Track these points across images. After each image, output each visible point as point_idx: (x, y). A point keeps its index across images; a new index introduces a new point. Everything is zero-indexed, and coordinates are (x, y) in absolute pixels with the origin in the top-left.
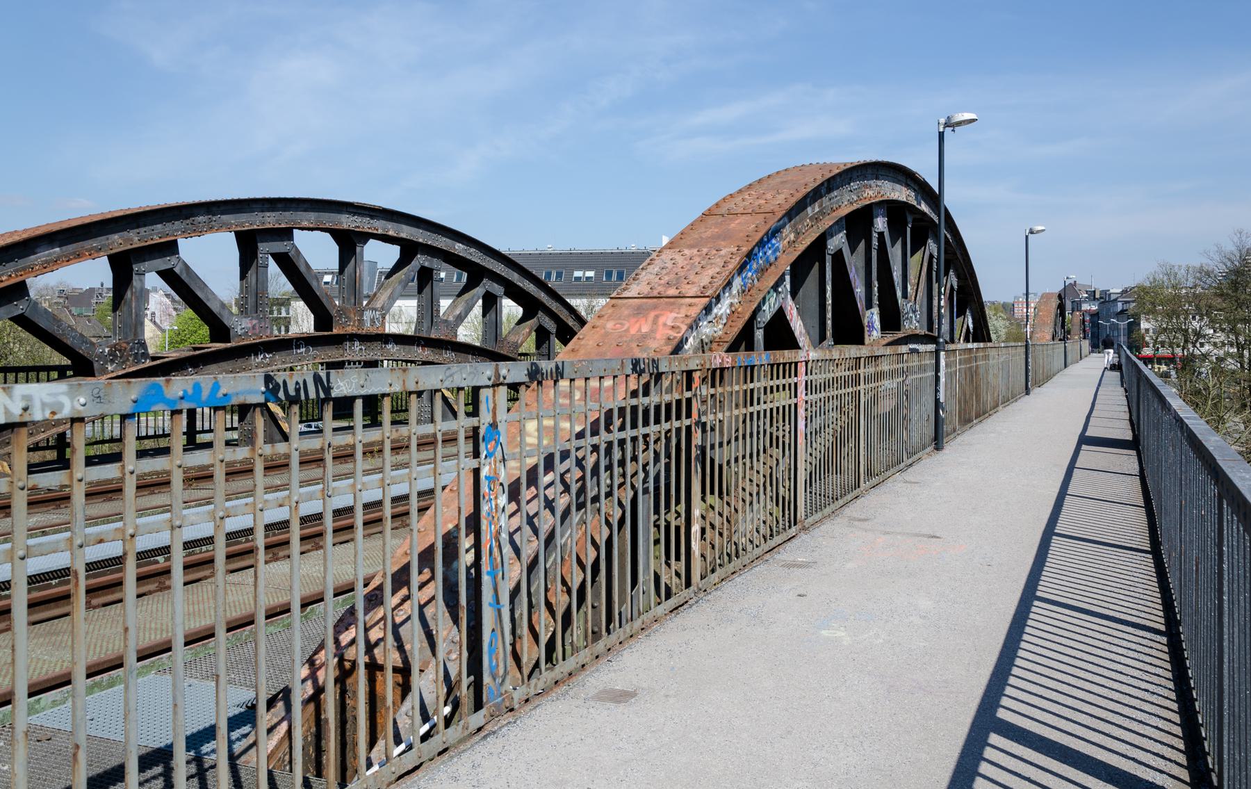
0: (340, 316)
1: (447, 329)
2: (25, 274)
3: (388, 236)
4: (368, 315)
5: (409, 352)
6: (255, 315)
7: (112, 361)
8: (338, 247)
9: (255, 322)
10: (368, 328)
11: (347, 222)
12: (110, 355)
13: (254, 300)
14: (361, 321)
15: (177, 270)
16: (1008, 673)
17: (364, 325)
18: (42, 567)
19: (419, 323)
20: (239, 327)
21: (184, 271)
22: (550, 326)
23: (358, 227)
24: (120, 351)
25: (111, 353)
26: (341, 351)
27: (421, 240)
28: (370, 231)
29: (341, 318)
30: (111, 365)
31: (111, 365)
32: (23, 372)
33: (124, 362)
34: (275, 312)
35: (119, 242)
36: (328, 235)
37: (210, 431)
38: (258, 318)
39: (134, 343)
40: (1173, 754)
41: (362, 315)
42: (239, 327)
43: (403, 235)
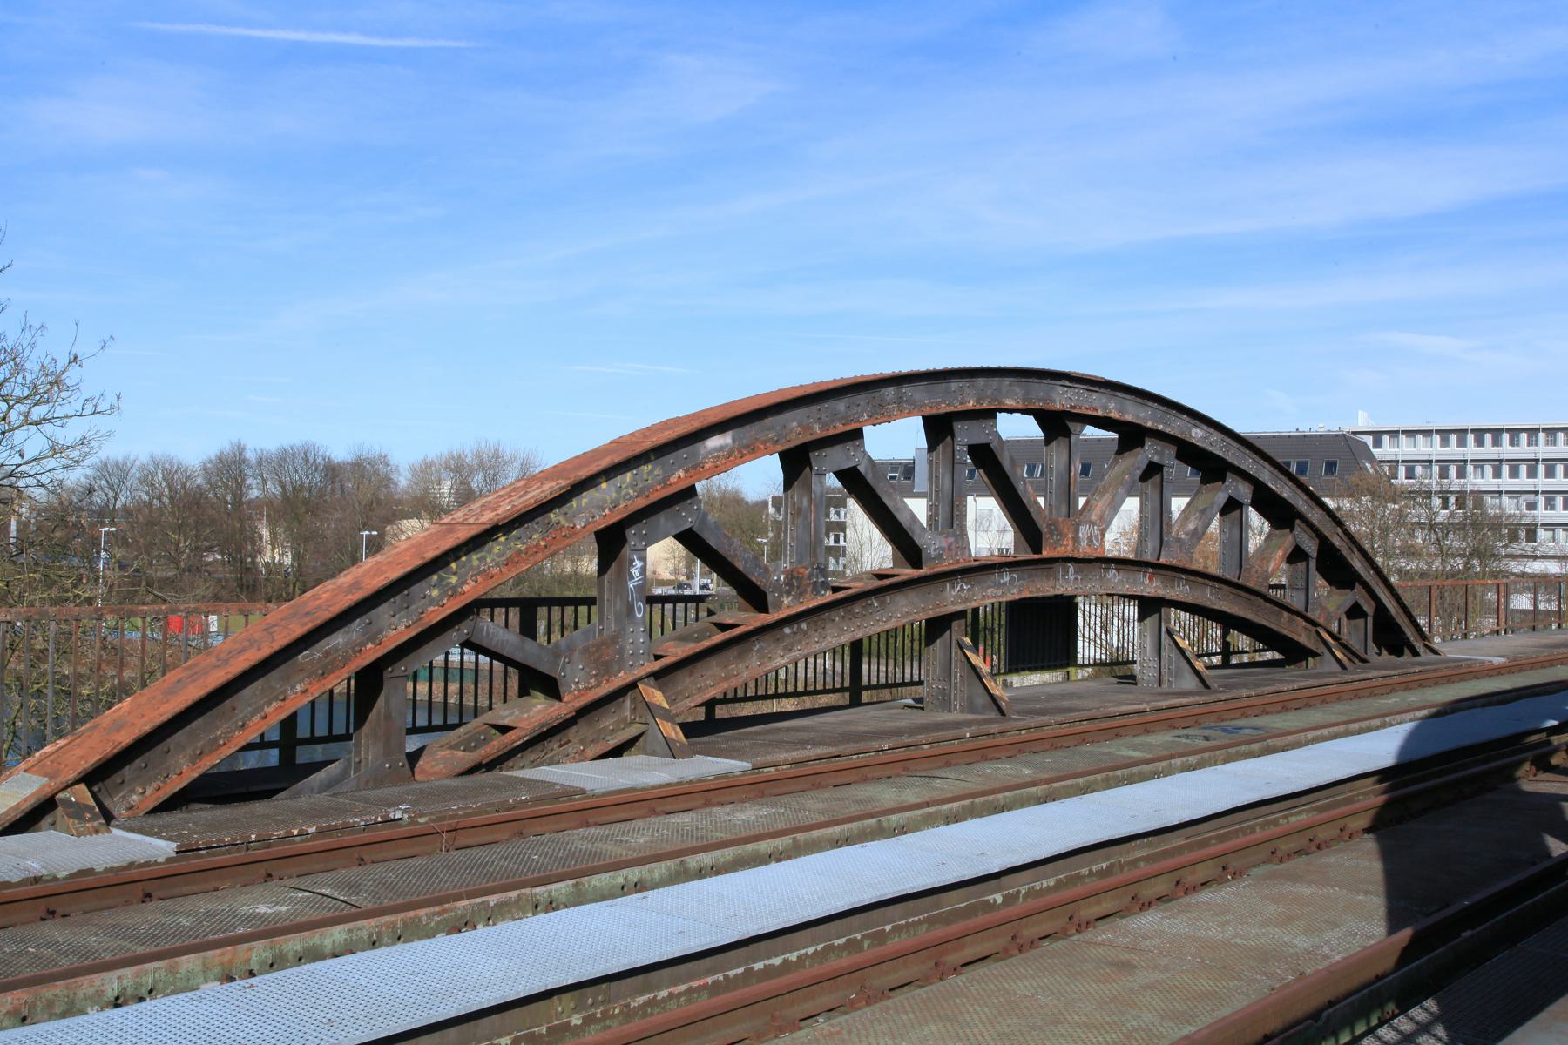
0: (1051, 533)
1: (1181, 551)
2: (695, 474)
3: (1110, 418)
4: (1084, 531)
5: (1134, 583)
6: (951, 530)
7: (788, 593)
8: (782, 475)
9: (951, 540)
10: (1084, 550)
11: (1062, 399)
12: (786, 585)
13: (948, 509)
14: (1076, 540)
15: (862, 469)
16: (768, 834)
17: (1079, 543)
18: (882, 892)
19: (1142, 539)
20: (932, 548)
21: (870, 471)
22: (1311, 547)
23: (1075, 407)
24: (797, 578)
25: (788, 583)
26: (1051, 582)
27: (1149, 424)
28: (1090, 413)
29: (1052, 535)
30: (787, 597)
31: (787, 597)
32: (584, 604)
33: (801, 594)
34: (832, 538)
35: (796, 427)
36: (1031, 419)
37: (920, 683)
38: (954, 535)
39: (813, 569)
40: (118, 726)
41: (1077, 531)
42: (932, 548)
43: (1128, 418)
